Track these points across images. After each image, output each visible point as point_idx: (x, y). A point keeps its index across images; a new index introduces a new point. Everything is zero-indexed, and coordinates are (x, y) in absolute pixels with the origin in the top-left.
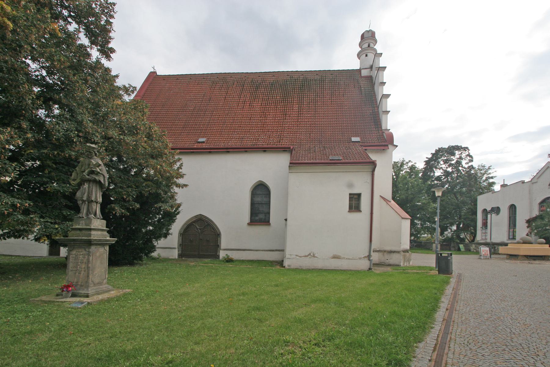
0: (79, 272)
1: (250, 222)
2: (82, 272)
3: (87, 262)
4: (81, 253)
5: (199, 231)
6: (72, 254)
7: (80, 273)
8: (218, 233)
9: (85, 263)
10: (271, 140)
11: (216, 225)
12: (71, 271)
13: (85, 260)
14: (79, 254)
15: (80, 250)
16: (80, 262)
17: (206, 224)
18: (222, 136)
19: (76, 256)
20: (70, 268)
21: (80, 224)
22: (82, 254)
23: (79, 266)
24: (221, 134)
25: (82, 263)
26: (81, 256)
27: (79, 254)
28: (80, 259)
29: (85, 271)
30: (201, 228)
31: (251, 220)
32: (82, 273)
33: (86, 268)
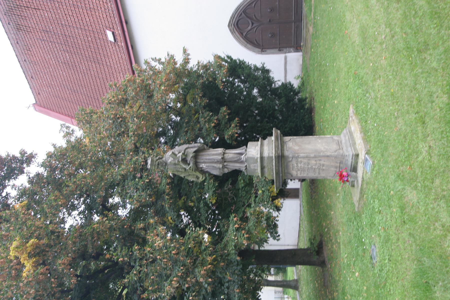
2: (322, 162)
4: (295, 165)
5: (254, 25)
7: (323, 165)
14: (295, 168)
17: (243, 15)
22: (297, 164)
26: (299, 165)
28: (303, 166)
29: (320, 160)
30: (251, 23)
33: (316, 159)
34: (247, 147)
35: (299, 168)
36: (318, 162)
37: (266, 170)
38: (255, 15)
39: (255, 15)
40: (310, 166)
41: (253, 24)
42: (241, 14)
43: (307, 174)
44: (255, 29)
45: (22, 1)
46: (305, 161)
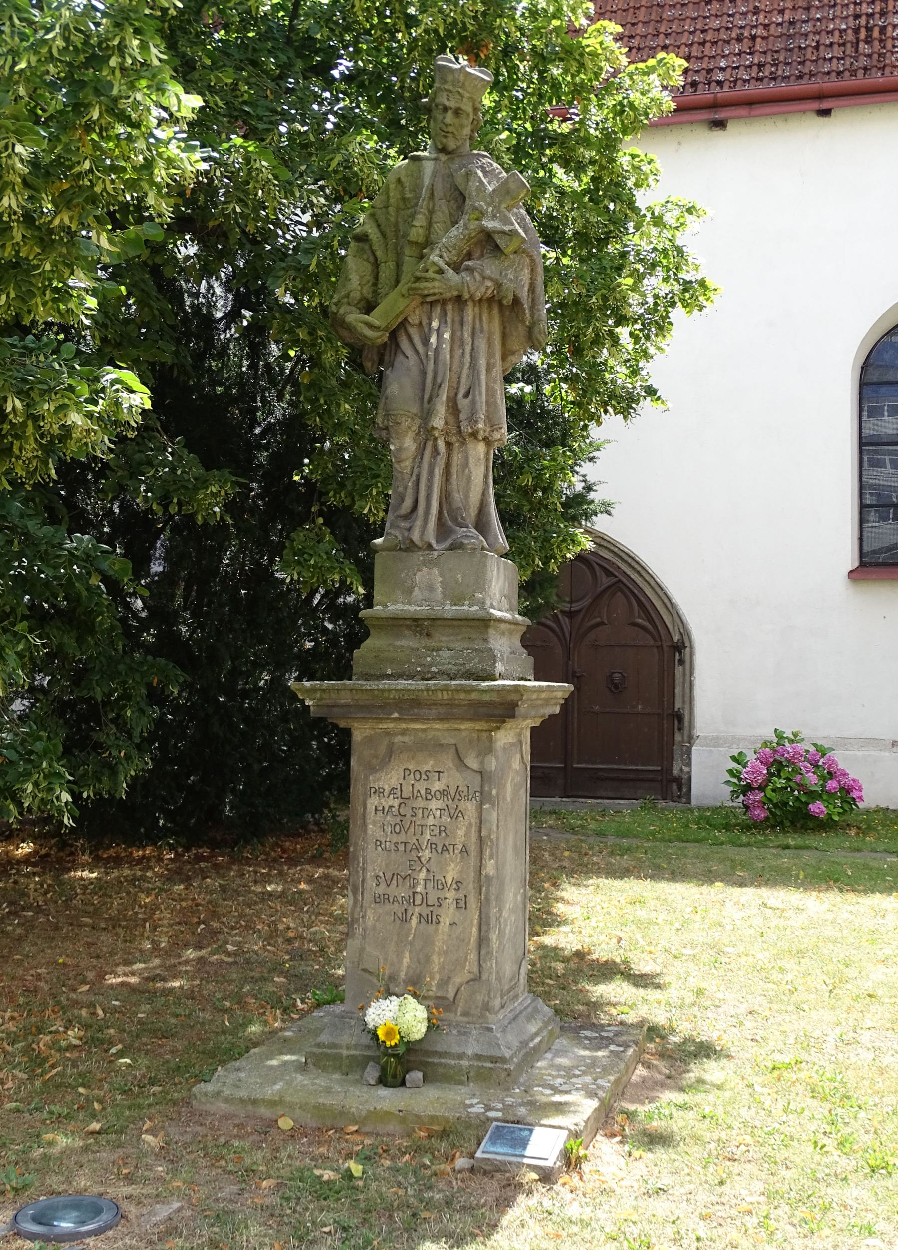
0: (425, 911)
1: (856, 564)
2: (447, 915)
3: (473, 848)
4: (437, 786)
5: (565, 621)
6: (379, 792)
7: (430, 919)
8: (676, 638)
9: (465, 851)
10: (722, 70)
11: (658, 588)
12: (378, 899)
13: (461, 833)
14: (421, 787)
15: (429, 765)
16: (432, 845)
17: (606, 581)
18: (667, 35)
19: (404, 801)
20: (371, 883)
21: (416, 591)
22: (444, 793)
23: (423, 875)
24: (660, 21)
25: (445, 848)
26: (434, 805)
27: (421, 787)
28: (431, 821)
29: (461, 904)
30: (575, 607)
31: (861, 554)
32: (445, 920)
33: (470, 886)
34: (506, 555)
35: (420, 803)
36: (451, 895)
37: (408, 642)
38: (602, 624)
39: (602, 624)
40: (426, 854)
41: (570, 614)
42: (609, 573)
43: (378, 843)
44: (646, 624)
45: (18, 9)
46: (461, 833)
